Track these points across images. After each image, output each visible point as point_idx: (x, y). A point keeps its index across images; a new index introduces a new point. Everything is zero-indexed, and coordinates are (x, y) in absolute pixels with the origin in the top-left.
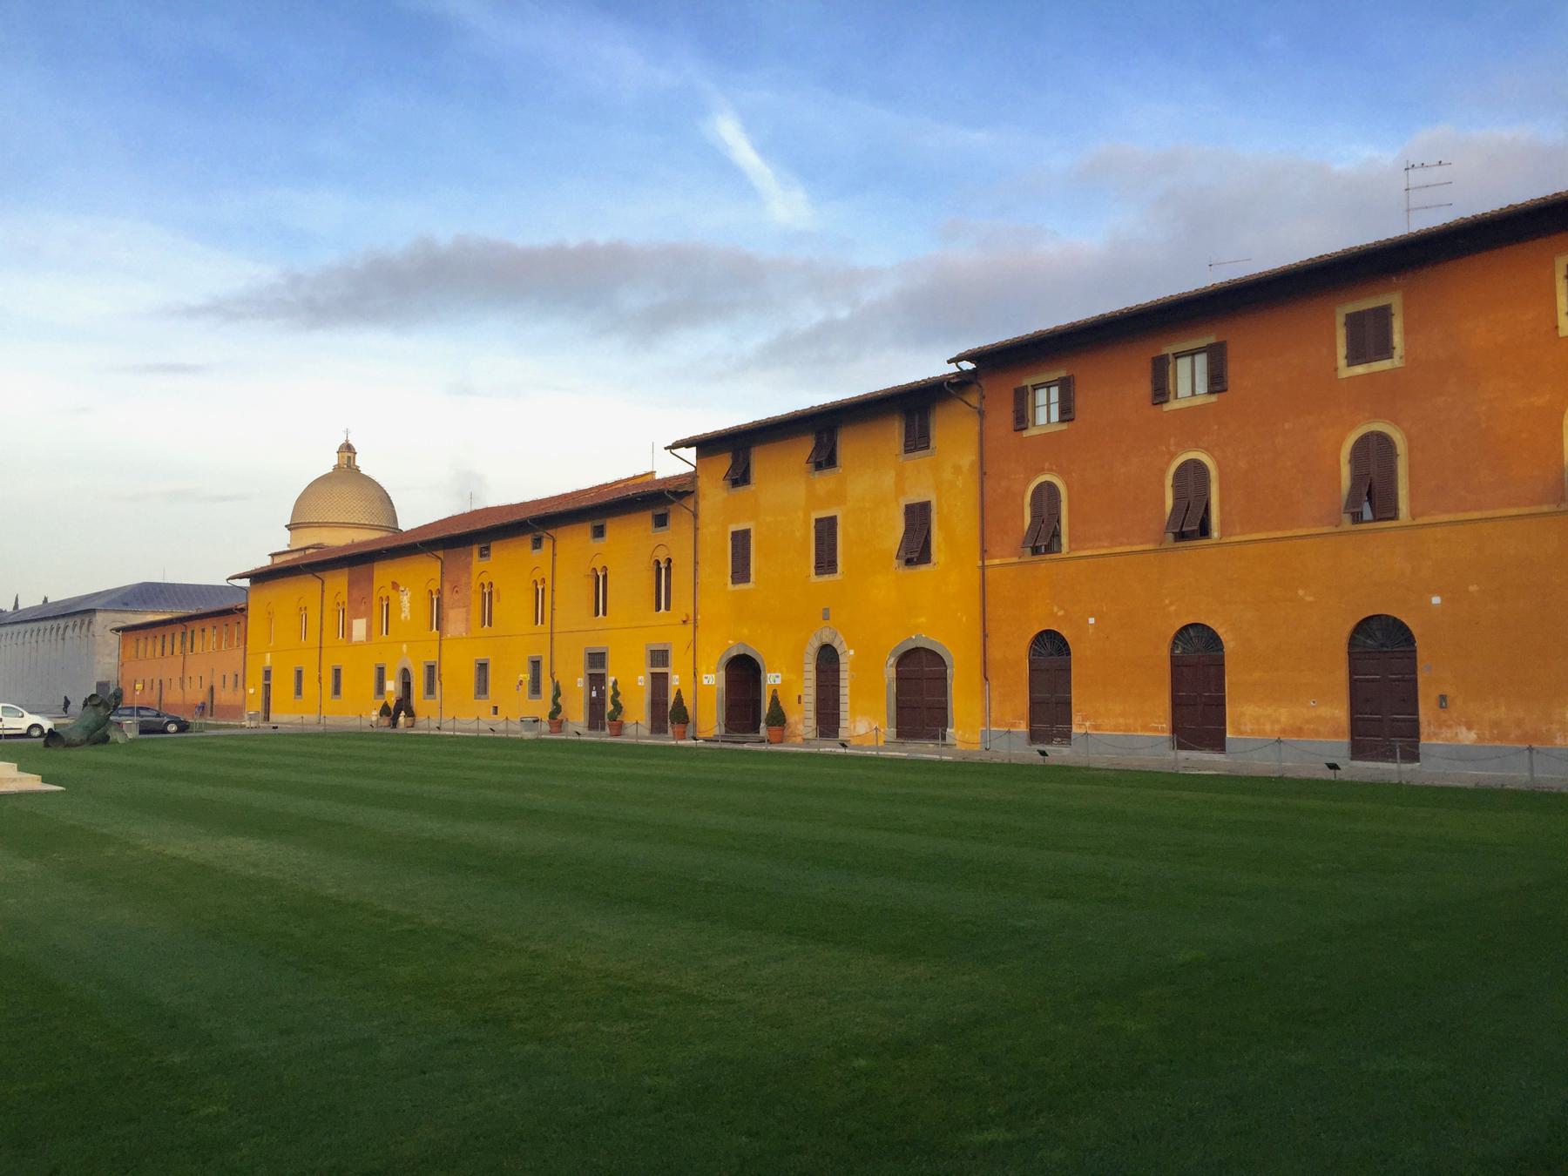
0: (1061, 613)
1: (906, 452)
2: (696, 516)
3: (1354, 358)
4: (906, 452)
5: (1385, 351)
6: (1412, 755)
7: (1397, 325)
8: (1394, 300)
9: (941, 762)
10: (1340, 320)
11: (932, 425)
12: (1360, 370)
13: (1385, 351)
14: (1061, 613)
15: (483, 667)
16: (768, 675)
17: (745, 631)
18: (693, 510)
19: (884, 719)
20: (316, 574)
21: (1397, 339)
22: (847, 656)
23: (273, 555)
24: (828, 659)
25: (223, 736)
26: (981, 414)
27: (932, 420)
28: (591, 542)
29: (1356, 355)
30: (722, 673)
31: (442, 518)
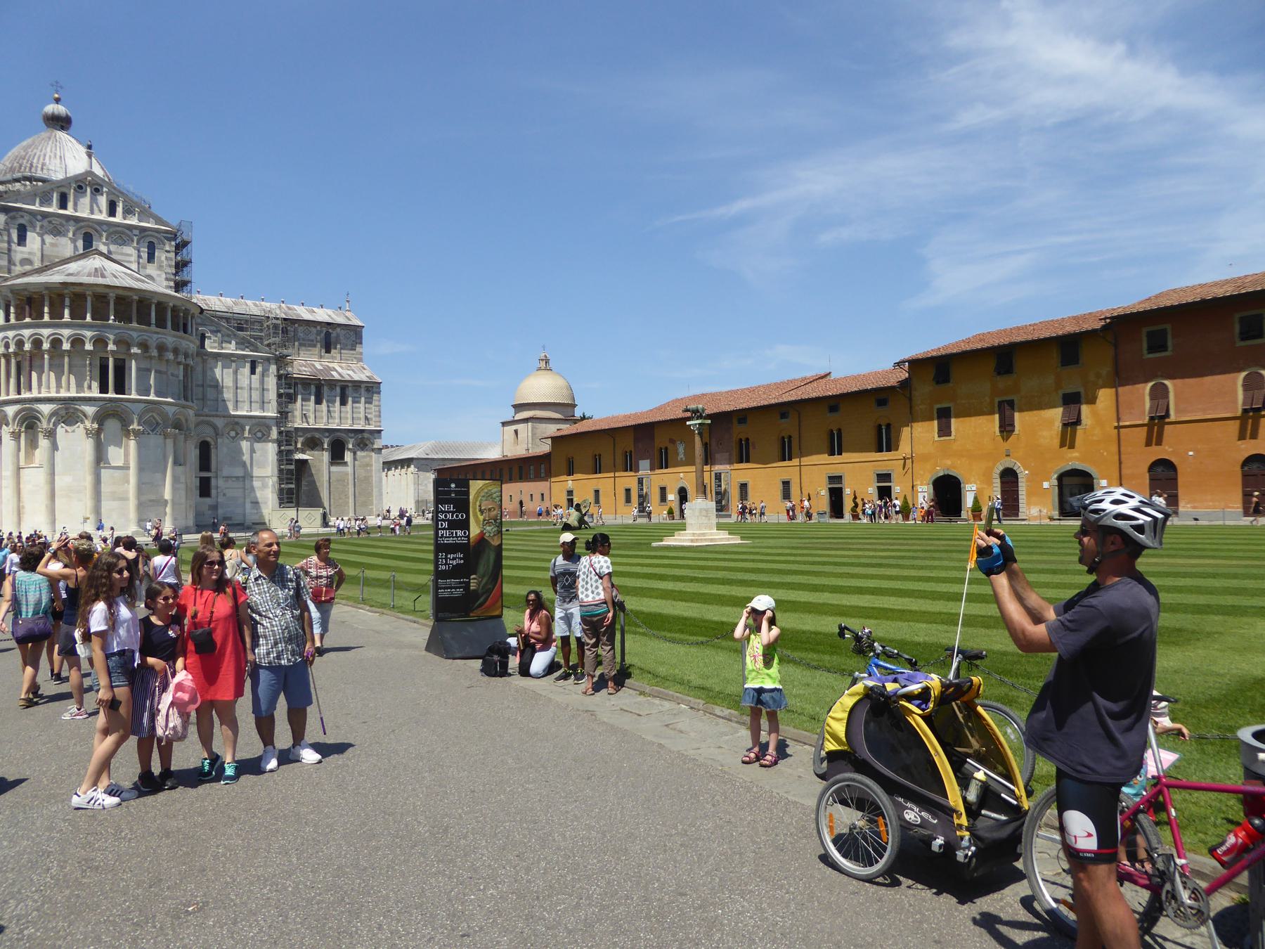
0: (1171, 450)
1: (1062, 366)
2: (910, 400)
4: (1062, 366)
8: (1168, 327)
9: (1224, 527)
12: (1151, 356)
13: (1243, 339)
14: (1171, 450)
15: (597, 492)
17: (949, 462)
18: (908, 395)
19: (1051, 507)
21: (1170, 343)
22: (1023, 473)
24: (1009, 477)
28: (828, 415)
29: (1151, 349)
30: (931, 486)
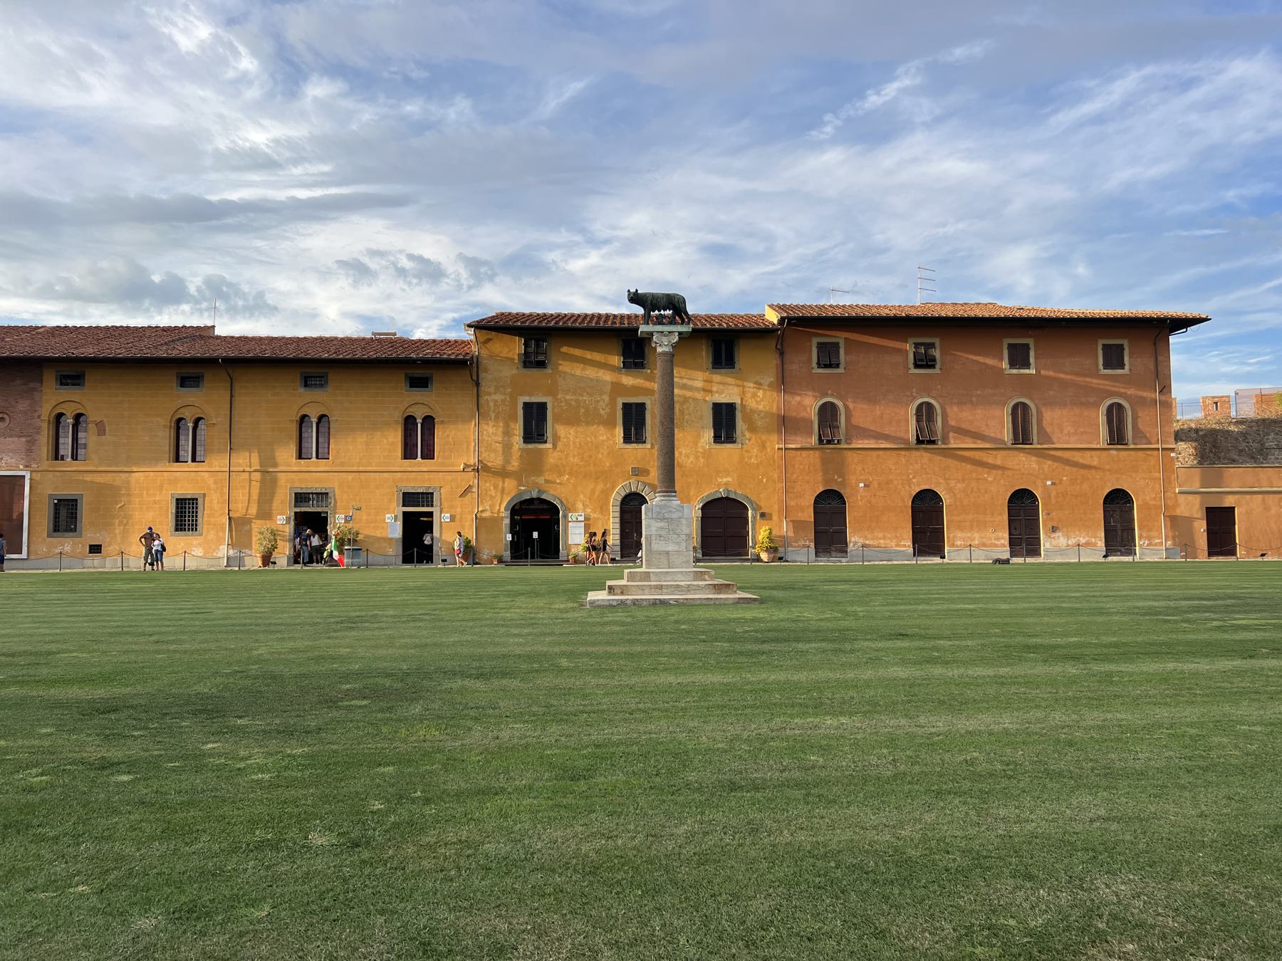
2: (478, 384)
3: (1106, 366)
5: (1026, 365)
6: (1131, 552)
7: (1032, 354)
10: (1100, 348)
11: (736, 354)
12: (1014, 371)
13: (1122, 366)
16: (570, 514)
20: (230, 371)
21: (1032, 360)
23: (373, 334)
25: (970, 598)
26: (782, 354)
27: (736, 349)
31: (327, 335)
